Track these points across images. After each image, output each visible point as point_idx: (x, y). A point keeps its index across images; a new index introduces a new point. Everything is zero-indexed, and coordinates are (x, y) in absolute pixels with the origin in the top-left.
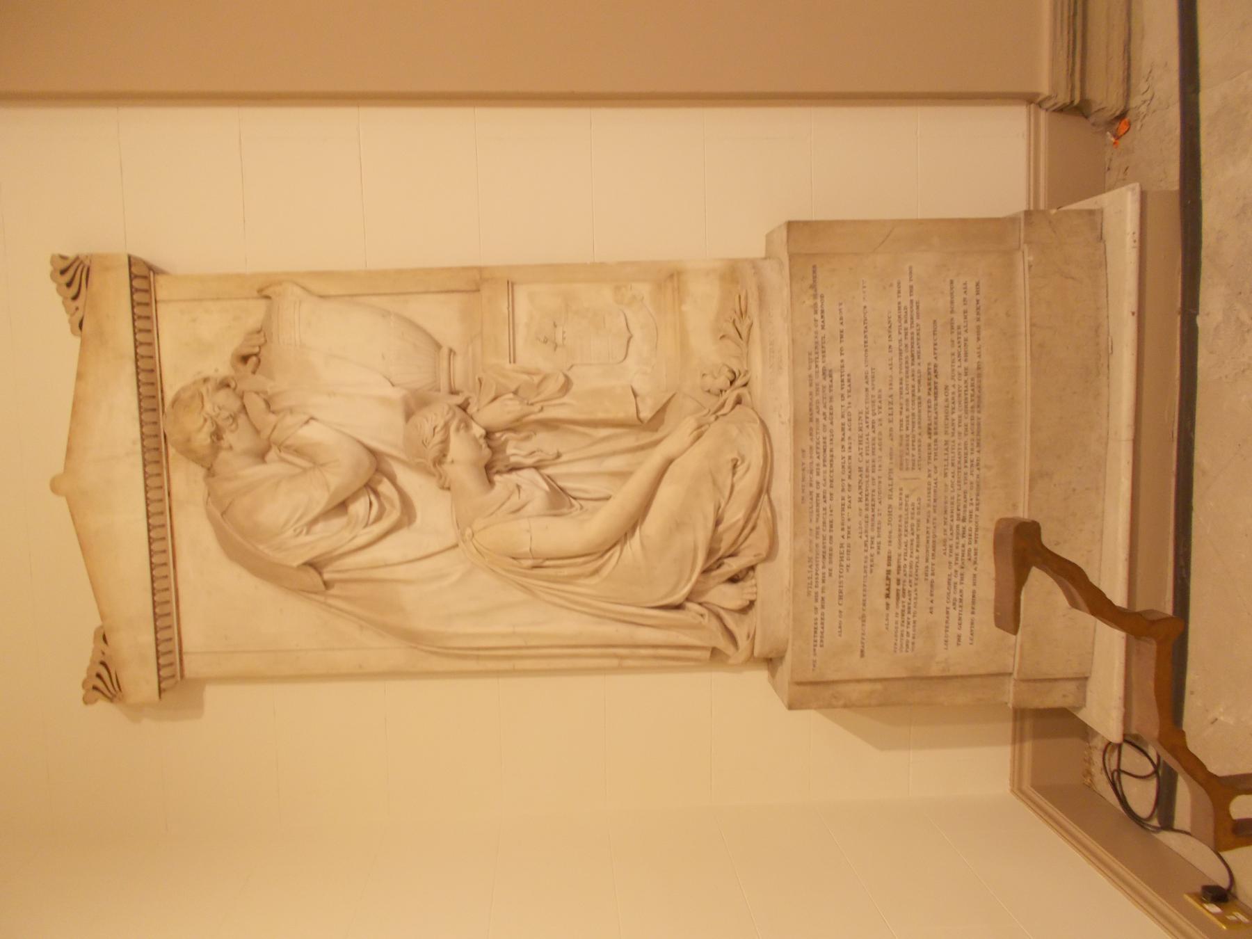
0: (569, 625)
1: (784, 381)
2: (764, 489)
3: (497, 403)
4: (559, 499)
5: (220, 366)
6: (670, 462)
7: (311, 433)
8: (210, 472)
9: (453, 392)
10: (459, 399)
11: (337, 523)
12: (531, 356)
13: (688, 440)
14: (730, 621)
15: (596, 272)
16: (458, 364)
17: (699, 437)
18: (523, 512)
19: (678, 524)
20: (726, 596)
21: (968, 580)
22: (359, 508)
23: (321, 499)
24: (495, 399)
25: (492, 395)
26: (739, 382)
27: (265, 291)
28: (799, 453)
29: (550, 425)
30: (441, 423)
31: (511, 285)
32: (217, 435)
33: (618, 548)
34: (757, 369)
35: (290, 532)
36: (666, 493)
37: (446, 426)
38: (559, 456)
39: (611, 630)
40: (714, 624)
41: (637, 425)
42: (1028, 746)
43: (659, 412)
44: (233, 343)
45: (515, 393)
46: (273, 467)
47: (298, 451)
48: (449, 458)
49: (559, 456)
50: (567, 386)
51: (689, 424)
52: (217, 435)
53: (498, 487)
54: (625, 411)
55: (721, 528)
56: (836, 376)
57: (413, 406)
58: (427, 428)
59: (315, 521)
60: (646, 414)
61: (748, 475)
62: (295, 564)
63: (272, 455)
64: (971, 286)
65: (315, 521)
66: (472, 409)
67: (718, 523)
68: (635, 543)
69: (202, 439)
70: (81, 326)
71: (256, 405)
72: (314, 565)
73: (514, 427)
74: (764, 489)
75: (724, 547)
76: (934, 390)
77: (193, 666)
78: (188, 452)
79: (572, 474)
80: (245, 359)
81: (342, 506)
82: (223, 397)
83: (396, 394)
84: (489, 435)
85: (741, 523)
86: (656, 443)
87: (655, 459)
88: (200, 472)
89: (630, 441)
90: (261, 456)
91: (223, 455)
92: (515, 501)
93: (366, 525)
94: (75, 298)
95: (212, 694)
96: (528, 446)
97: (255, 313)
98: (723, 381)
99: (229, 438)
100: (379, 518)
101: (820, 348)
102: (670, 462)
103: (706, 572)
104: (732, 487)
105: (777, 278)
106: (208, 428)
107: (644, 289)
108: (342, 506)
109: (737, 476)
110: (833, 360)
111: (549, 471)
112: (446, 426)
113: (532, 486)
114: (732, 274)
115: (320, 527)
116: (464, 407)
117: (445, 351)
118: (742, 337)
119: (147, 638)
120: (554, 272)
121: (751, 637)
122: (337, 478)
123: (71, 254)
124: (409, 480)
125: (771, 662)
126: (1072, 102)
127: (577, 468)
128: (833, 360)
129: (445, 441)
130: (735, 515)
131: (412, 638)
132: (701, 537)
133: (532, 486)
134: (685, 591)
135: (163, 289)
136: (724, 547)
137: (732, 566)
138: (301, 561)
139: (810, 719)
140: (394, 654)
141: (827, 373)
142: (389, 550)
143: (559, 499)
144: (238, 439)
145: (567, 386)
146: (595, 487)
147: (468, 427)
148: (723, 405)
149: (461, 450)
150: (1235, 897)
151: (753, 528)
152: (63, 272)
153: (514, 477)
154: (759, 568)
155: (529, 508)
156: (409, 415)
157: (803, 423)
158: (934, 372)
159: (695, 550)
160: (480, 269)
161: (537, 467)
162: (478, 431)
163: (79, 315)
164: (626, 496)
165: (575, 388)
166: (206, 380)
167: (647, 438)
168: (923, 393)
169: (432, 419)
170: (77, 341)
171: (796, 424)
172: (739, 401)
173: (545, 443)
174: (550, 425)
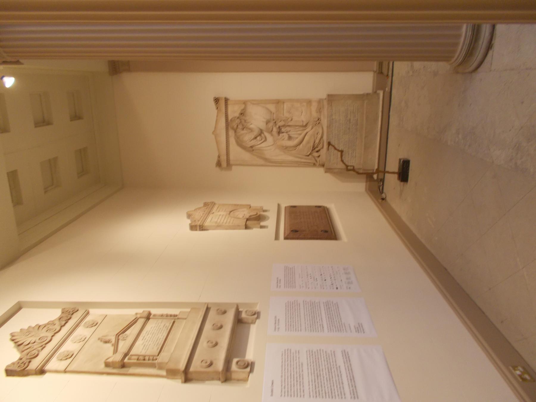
0: (290, 158)
1: (326, 120)
2: (322, 137)
3: (280, 122)
4: (290, 138)
5: (237, 115)
6: (307, 133)
7: (252, 126)
8: (235, 132)
9: (274, 120)
10: (274, 121)
11: (255, 140)
12: (286, 115)
13: (310, 129)
14: (316, 158)
15: (298, 101)
16: (275, 115)
17: (312, 129)
18: (284, 140)
19: (308, 142)
20: (316, 154)
21: (354, 153)
22: (258, 138)
23: (253, 137)
24: (280, 121)
25: (280, 121)
26: (319, 120)
27: (245, 103)
28: (328, 132)
29: (289, 126)
30: (272, 125)
31: (284, 103)
32: (237, 126)
33: (299, 146)
34: (322, 118)
35: (248, 142)
36: (307, 138)
37: (273, 125)
38: (290, 131)
39: (299, 160)
40: (314, 159)
41: (302, 126)
42: (368, 183)
43: (306, 125)
44: (239, 112)
45: (284, 120)
46: (245, 131)
47: (250, 129)
48: (273, 131)
49: (290, 131)
50: (292, 120)
51: (311, 127)
52: (237, 126)
53: (280, 136)
54: (301, 124)
55: (315, 143)
56: (334, 120)
57: (268, 122)
58: (270, 126)
59: (251, 140)
60: (304, 124)
61: (320, 135)
62: (249, 146)
63: (245, 129)
64: (357, 105)
65: (251, 140)
66: (277, 123)
67: (314, 142)
68: (301, 145)
69: (235, 127)
70: (217, 108)
71: (243, 121)
72: (252, 147)
73: (284, 126)
74: (322, 137)
75: (316, 146)
76: (350, 122)
77: (231, 162)
78: (233, 128)
79: (292, 133)
80: (242, 114)
81: (256, 138)
82: (238, 120)
83: (265, 120)
84: (279, 127)
85: (318, 142)
86: (305, 130)
87: (305, 132)
88: (234, 132)
89: (302, 129)
90: (243, 129)
91: (238, 129)
92: (283, 138)
93: (259, 141)
94: (217, 104)
95: (234, 168)
96: (286, 129)
97: (243, 107)
98: (317, 119)
99: (239, 126)
100: (261, 140)
101: (332, 115)
102: (307, 133)
103: (312, 150)
104: (317, 137)
105: (325, 103)
106: (236, 125)
107: (305, 104)
108: (256, 138)
109: (318, 135)
110: (334, 117)
111: (289, 133)
112: (273, 125)
113: (285, 136)
114: (320, 101)
115: (252, 141)
116: (275, 122)
117: (272, 113)
118: (320, 112)
119: (225, 157)
120: (291, 100)
121: (319, 161)
122: (256, 133)
123: (217, 97)
124: (267, 134)
125: (323, 166)
126: (303, 124)
127: (293, 133)
128: (334, 117)
129: (273, 128)
130: (317, 141)
131: (266, 160)
132: (312, 144)
133: (285, 136)
134: (309, 153)
135: (229, 102)
136: (316, 146)
137: (317, 149)
138: (250, 146)
139: (328, 175)
140: (262, 162)
141: (333, 119)
142: (263, 145)
143: (290, 138)
144: (240, 127)
145: (292, 120)
146: (296, 136)
147: (276, 126)
148: (316, 124)
149: (275, 130)
150: (386, 200)
151: (320, 144)
152: (215, 100)
153: (283, 134)
154: (321, 150)
155: (285, 139)
156: (267, 124)
157: (329, 127)
158: (350, 120)
159: (311, 147)
160: (279, 100)
161: (287, 132)
162: (277, 126)
163: (217, 107)
164: (301, 137)
165: (293, 120)
166: (235, 117)
167: (304, 128)
168: (348, 123)
169: (271, 125)
170: (216, 111)
171: (327, 127)
172: (319, 123)
173: (288, 129)
174: (289, 126)
